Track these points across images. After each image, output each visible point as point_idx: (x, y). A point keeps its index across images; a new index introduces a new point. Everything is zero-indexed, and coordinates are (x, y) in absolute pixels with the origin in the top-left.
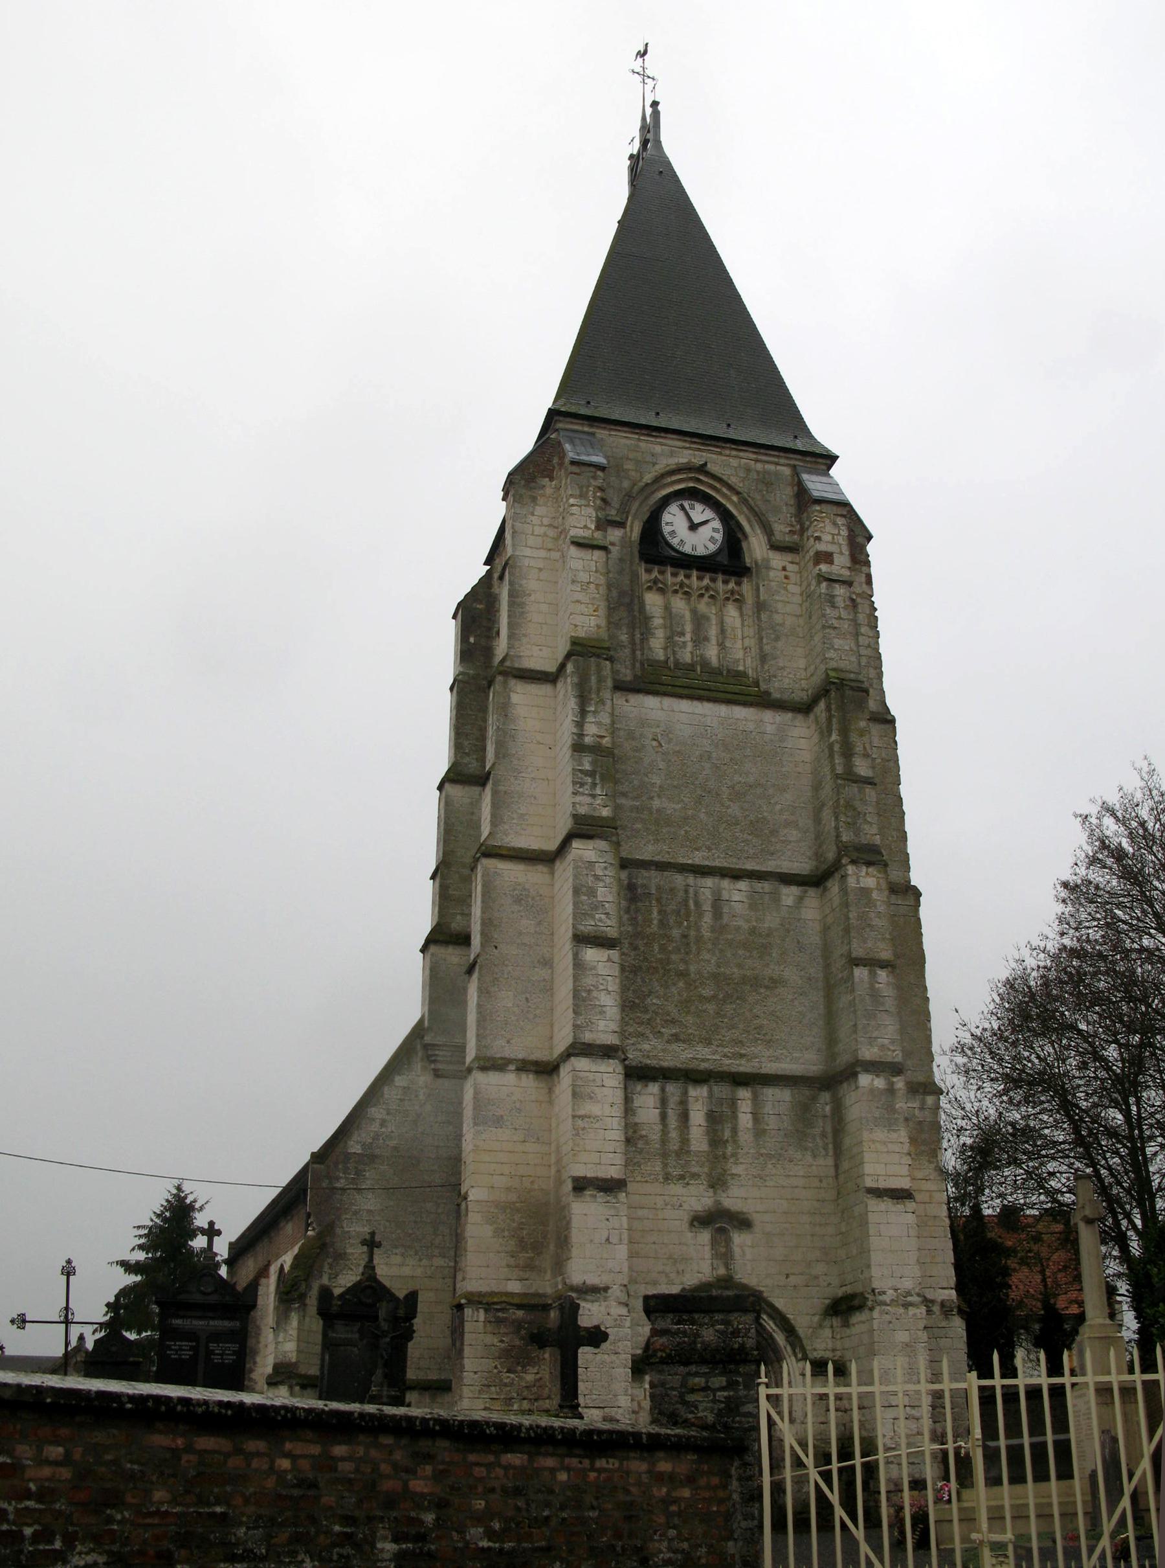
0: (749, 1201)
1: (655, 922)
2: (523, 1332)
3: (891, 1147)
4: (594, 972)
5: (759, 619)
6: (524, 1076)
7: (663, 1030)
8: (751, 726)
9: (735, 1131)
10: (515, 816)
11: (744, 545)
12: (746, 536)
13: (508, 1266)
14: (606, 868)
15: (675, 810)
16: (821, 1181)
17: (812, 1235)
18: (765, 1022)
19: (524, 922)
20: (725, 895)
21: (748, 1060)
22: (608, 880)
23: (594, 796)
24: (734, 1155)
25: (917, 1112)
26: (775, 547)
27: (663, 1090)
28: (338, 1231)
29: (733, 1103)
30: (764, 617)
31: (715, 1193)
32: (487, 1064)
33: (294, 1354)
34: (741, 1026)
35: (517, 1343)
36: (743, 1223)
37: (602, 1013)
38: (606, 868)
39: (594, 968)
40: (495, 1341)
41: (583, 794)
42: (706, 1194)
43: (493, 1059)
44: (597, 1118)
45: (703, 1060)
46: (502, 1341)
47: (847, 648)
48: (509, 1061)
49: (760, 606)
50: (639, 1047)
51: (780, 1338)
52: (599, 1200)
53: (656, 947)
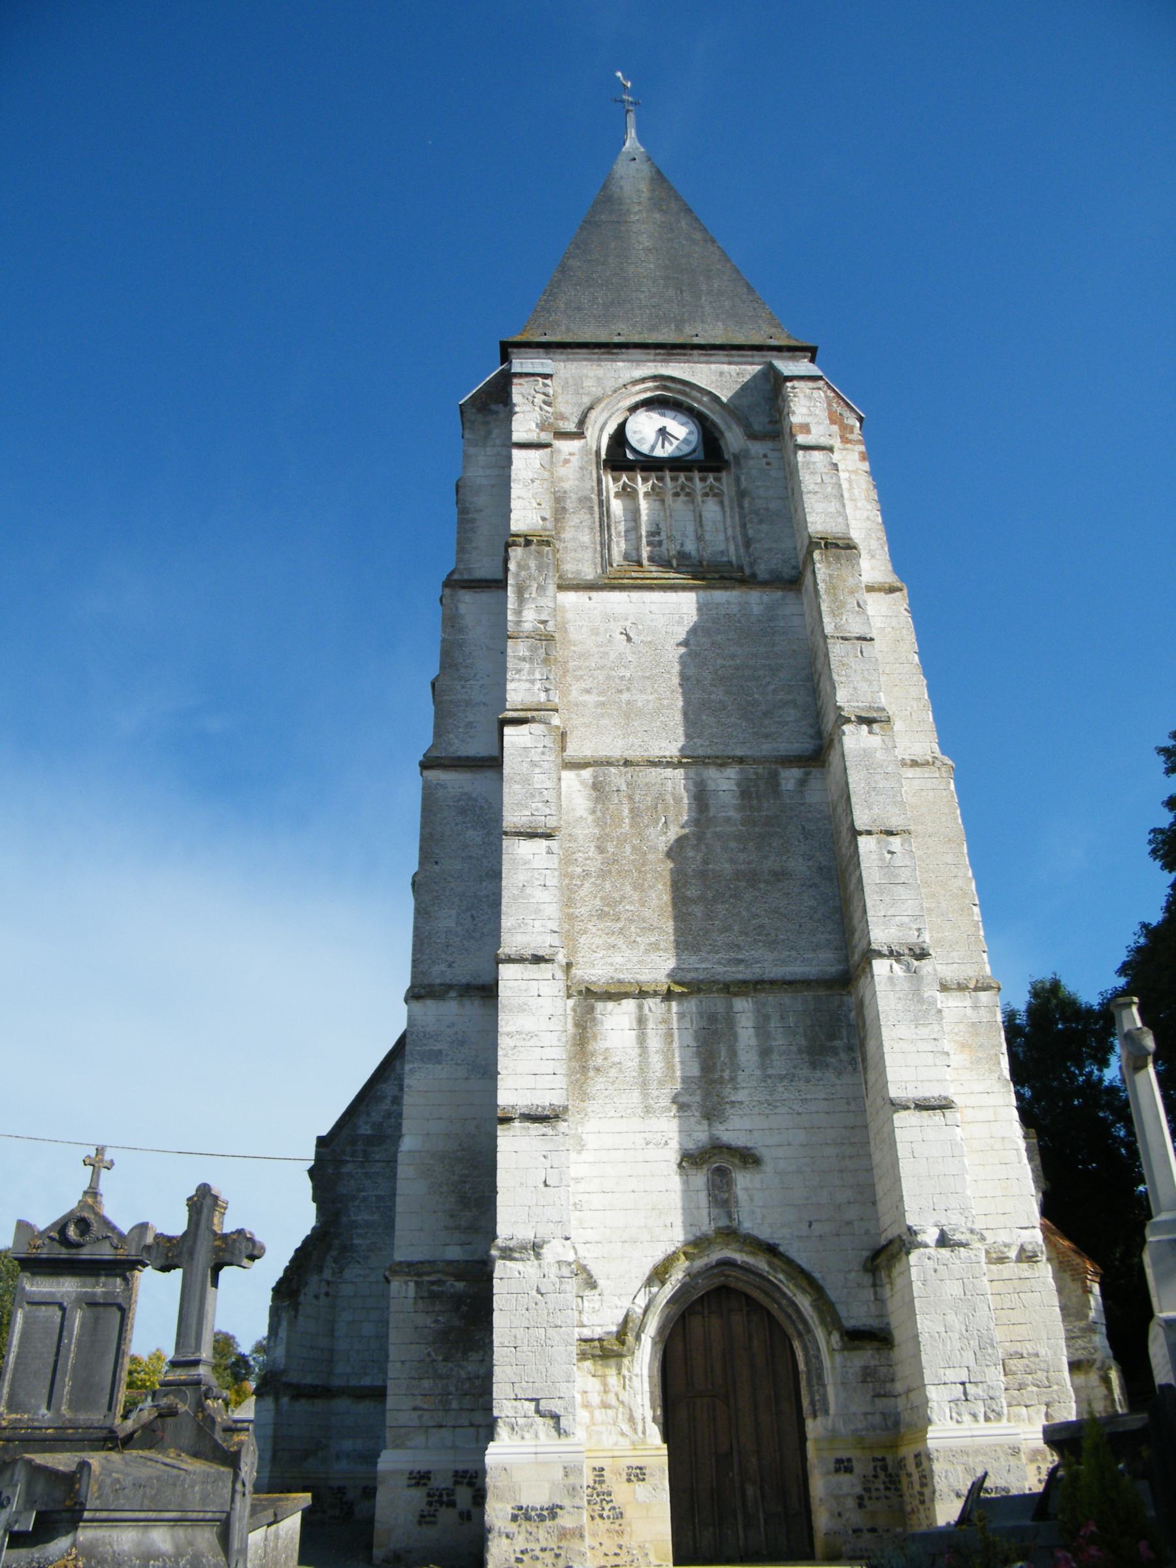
0: (756, 1133)
1: (627, 821)
2: (464, 1308)
3: (922, 1046)
4: (527, 866)
5: (741, 506)
6: (468, 1003)
7: (638, 939)
8: (735, 609)
9: (733, 1053)
10: (461, 725)
11: (722, 443)
12: (722, 433)
13: (446, 1228)
14: (543, 753)
15: (648, 701)
16: (848, 1103)
17: (841, 1171)
18: (766, 921)
19: (470, 833)
20: (711, 786)
21: (746, 967)
22: (546, 765)
23: (533, 682)
24: (732, 1079)
25: (969, 1011)
26: (752, 436)
27: (640, 1007)
28: (344, 1219)
29: (730, 1020)
30: (746, 504)
31: (710, 1125)
32: (423, 992)
33: (283, 1361)
34: (736, 928)
35: (457, 1322)
36: (748, 1158)
37: (538, 911)
38: (543, 753)
39: (529, 862)
40: (429, 1321)
41: (520, 680)
42: (698, 1127)
43: (431, 986)
44: (532, 1035)
45: (689, 970)
46: (436, 1321)
47: (832, 510)
48: (449, 987)
49: (742, 494)
50: (609, 960)
51: (804, 1302)
52: (533, 1132)
53: (628, 849)
